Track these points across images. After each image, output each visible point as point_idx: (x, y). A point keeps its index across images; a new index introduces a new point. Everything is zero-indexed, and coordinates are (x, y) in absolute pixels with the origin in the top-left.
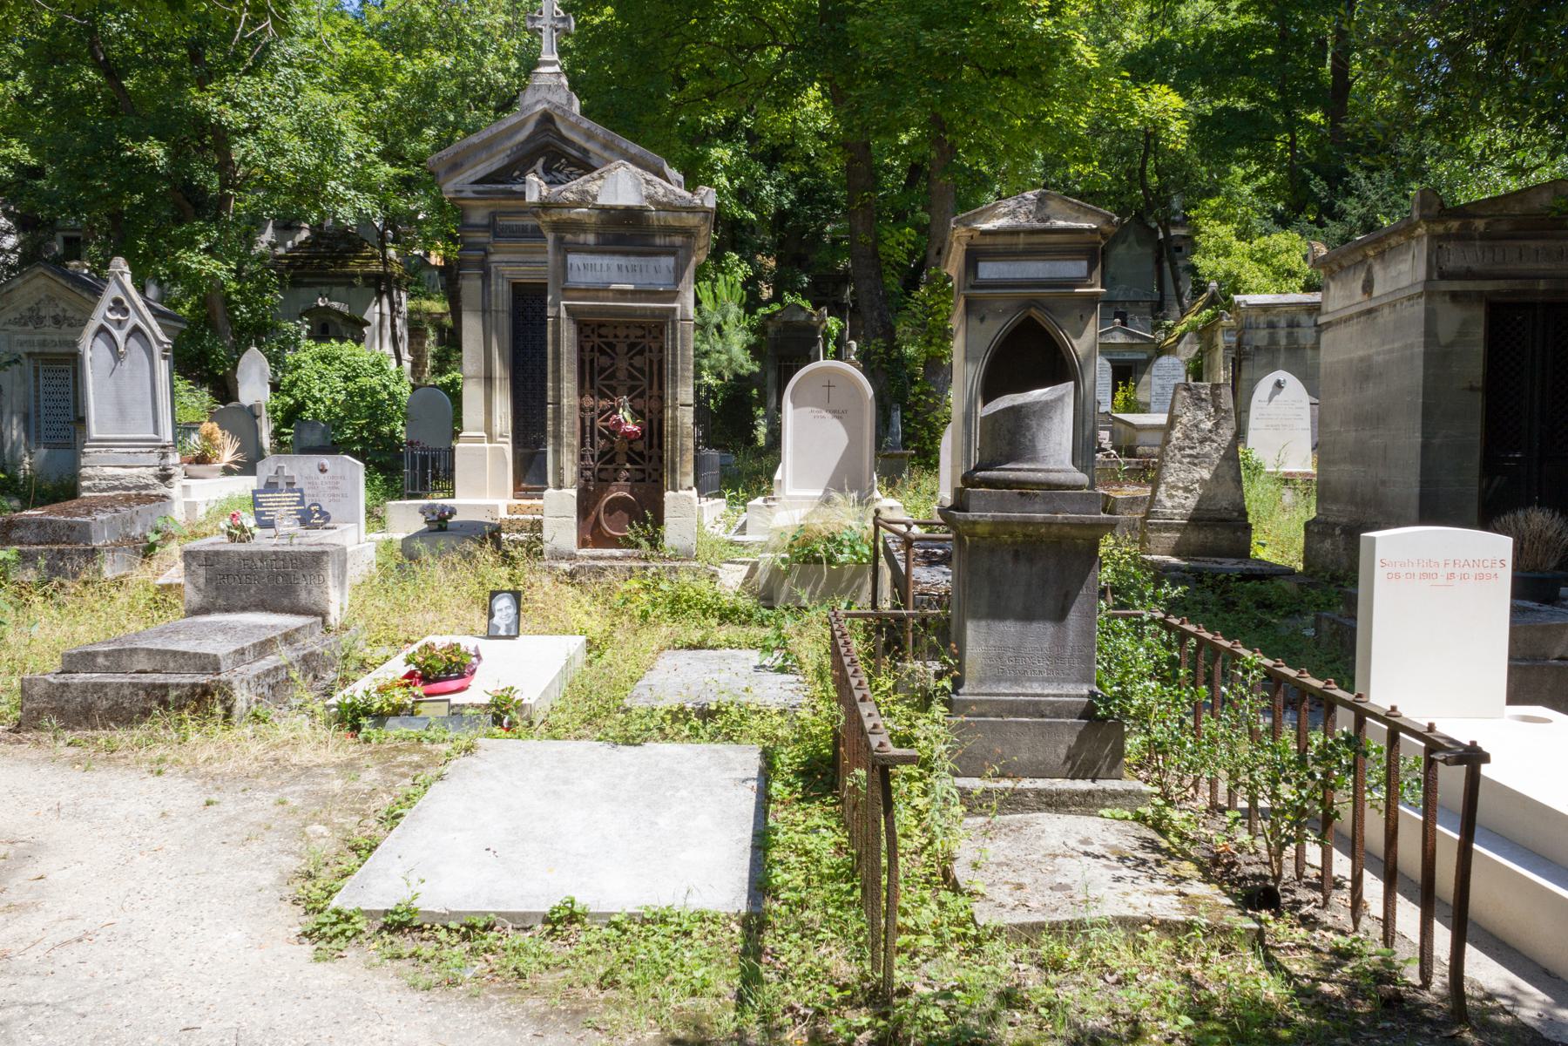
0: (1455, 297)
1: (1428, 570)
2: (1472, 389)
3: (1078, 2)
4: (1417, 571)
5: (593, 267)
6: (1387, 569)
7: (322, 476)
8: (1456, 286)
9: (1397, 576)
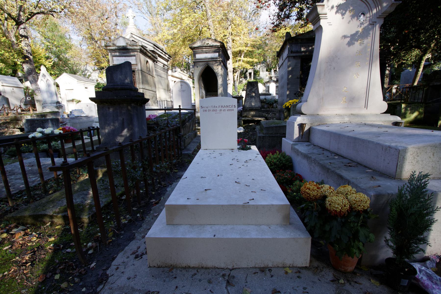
0: (294, 57)
1: (214, 109)
2: (298, 78)
4: (212, 109)
5: (119, 60)
7: (273, 278)
8: (294, 55)
9: (206, 111)
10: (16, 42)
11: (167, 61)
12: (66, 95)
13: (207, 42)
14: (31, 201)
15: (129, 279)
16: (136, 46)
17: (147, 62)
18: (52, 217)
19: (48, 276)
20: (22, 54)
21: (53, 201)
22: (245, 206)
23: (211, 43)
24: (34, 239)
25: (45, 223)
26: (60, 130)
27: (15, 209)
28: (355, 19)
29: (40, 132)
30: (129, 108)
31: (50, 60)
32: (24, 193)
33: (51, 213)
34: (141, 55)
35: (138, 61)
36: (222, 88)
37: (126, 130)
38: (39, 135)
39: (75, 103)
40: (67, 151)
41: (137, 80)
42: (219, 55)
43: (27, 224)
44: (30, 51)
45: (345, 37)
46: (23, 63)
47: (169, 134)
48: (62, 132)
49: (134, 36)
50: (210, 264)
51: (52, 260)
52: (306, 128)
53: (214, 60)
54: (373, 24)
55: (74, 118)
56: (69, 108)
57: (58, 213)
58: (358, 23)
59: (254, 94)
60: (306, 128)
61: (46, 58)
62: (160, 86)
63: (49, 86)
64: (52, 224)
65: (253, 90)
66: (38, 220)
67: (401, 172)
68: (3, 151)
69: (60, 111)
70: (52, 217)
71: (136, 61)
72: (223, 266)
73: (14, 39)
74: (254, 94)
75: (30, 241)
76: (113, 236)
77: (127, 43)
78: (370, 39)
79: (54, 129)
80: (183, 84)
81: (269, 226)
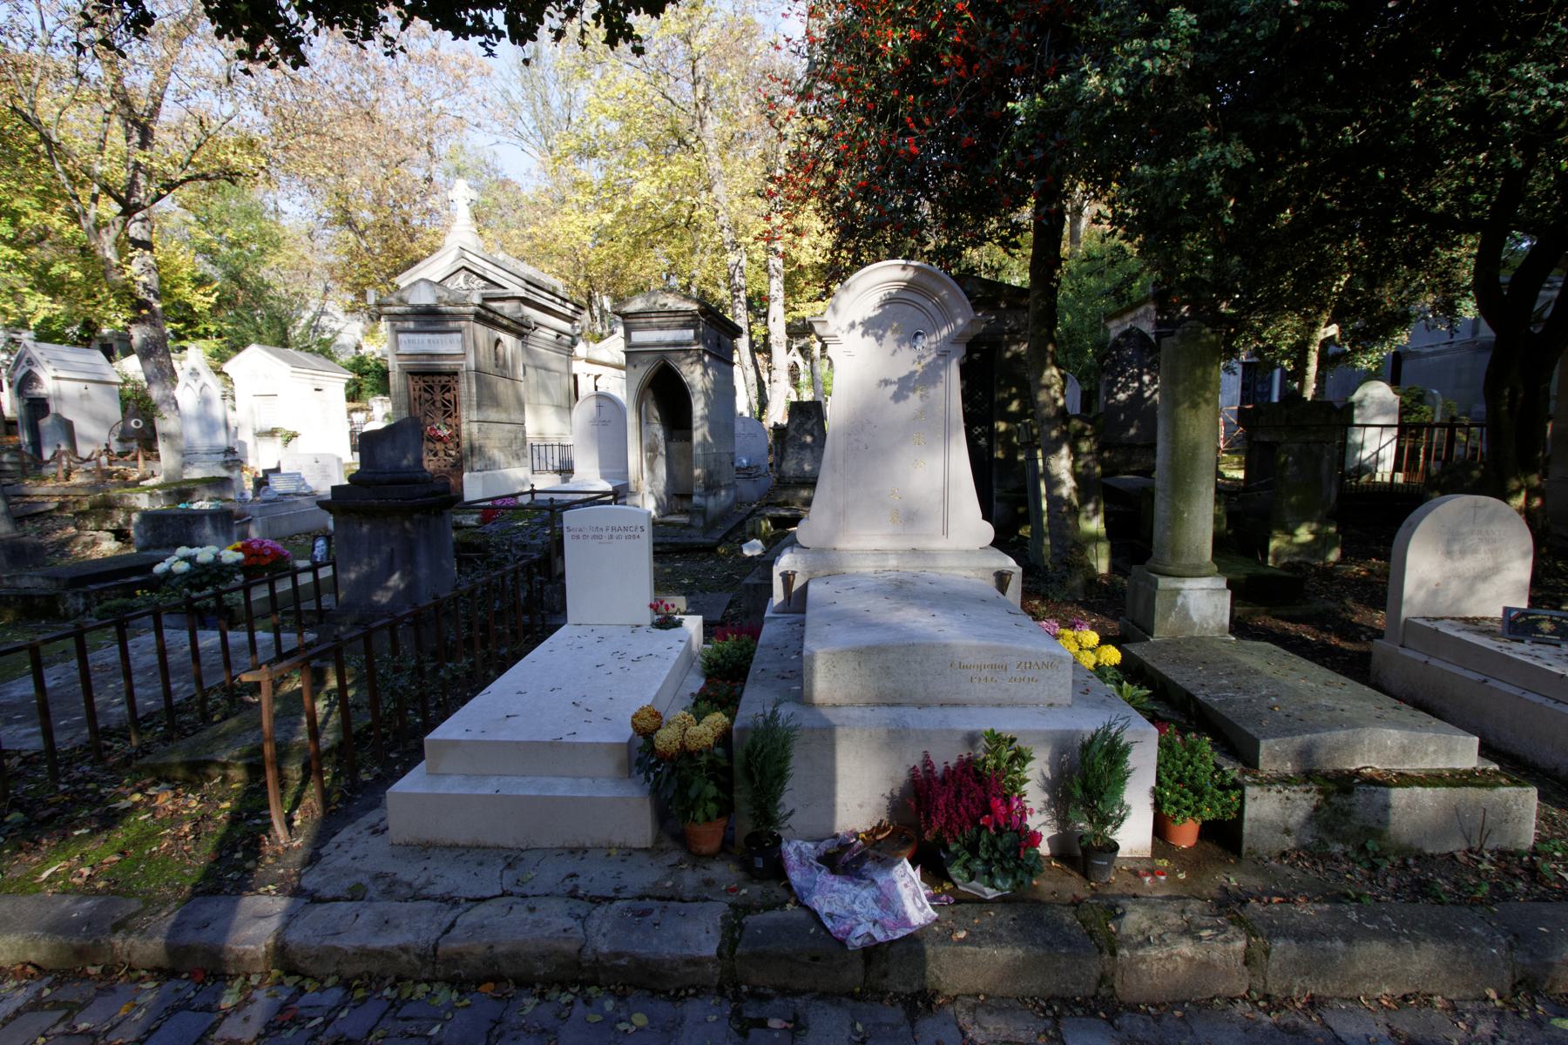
4: (591, 533)
10: (115, 261)
11: (571, 320)
12: (252, 411)
13: (662, 300)
14: (175, 736)
15: (354, 859)
16: (465, 305)
17: (498, 341)
18: (225, 766)
19: (224, 853)
20: (132, 295)
21: (225, 736)
22: (555, 745)
23: (672, 302)
24: (194, 804)
25: (210, 779)
26: (236, 550)
27: (145, 750)
28: (906, 349)
29: (184, 559)
30: (407, 525)
31: (209, 289)
32: (156, 719)
33: (224, 758)
34: (478, 326)
35: (470, 344)
36: (706, 429)
37: (396, 576)
38: (183, 567)
39: (279, 441)
40: (255, 608)
41: (463, 398)
42: (696, 336)
43: (175, 779)
44: (155, 286)
45: (886, 382)
46: (133, 321)
47: (515, 579)
48: (240, 556)
49: (468, 255)
50: (490, 841)
51: (229, 832)
52: (797, 584)
53: (679, 346)
54: (944, 354)
55: (274, 501)
56: (261, 457)
57: (239, 758)
58: (914, 354)
59: (809, 439)
60: (797, 584)
61: (195, 280)
62: (543, 399)
63: (206, 401)
64: (225, 779)
65: (808, 426)
66: (195, 773)
67: (811, 692)
68: (82, 608)
69: (235, 474)
70: (225, 766)
71: (464, 347)
72: (511, 844)
73: (110, 254)
74: (809, 439)
75: (187, 807)
76: (340, 801)
77: (439, 298)
78: (941, 387)
79: (222, 549)
80: (603, 402)
81: (593, 779)
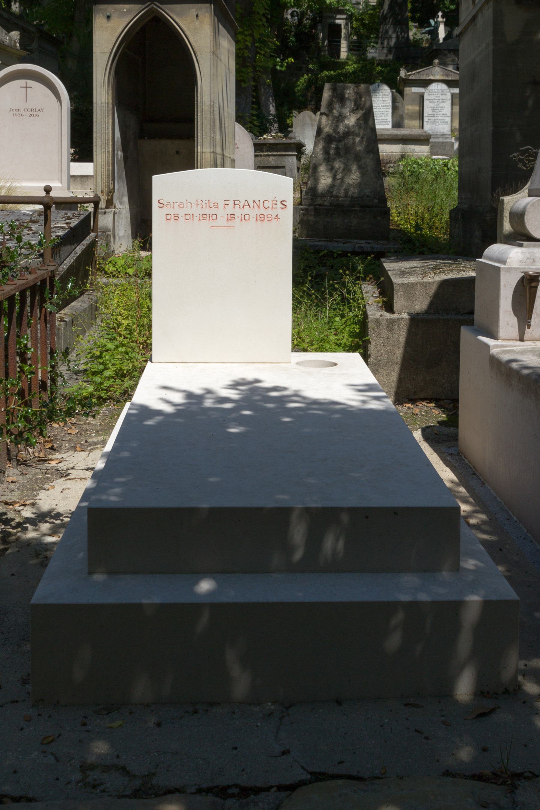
1: (207, 211)
3: (539, 345)
4: (197, 211)
6: (165, 210)
